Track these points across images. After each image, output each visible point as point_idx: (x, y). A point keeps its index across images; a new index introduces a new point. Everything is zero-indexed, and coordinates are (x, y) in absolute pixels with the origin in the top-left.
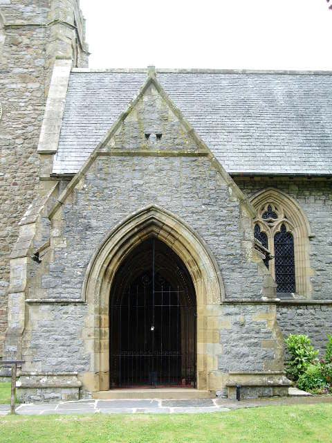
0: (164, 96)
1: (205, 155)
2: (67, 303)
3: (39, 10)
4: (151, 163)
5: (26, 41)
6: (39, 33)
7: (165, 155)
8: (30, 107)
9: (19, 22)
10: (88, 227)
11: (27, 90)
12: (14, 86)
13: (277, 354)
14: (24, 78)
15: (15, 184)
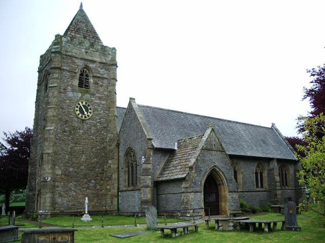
0: (215, 135)
1: (224, 151)
2: (198, 192)
3: (106, 72)
4: (214, 153)
5: (101, 83)
6: (105, 81)
7: (216, 151)
8: (102, 111)
9: (98, 75)
10: (201, 170)
11: (101, 103)
12: (96, 101)
13: (239, 205)
14: (100, 98)
15: (97, 142)
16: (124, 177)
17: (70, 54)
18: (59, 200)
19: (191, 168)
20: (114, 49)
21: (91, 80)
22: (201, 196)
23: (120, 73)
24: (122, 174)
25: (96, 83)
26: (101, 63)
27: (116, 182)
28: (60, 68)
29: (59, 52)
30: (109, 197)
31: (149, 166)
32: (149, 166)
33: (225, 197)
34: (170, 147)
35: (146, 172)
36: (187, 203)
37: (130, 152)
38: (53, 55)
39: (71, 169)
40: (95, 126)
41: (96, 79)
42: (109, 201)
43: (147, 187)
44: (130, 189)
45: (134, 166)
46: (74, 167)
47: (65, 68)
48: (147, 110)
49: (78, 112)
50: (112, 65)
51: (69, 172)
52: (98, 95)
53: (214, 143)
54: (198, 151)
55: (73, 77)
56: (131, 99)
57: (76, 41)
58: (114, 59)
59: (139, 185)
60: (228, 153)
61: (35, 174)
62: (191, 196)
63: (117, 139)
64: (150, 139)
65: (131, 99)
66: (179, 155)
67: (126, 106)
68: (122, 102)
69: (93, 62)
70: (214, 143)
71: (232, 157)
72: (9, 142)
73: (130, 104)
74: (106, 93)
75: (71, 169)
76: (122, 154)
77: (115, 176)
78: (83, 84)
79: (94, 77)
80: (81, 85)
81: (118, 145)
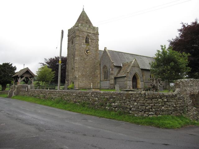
4: (136, 68)
6: (95, 41)
14: (93, 47)
16: (102, 76)
17: (82, 30)
18: (80, 84)
19: (128, 73)
20: (98, 28)
21: (90, 40)
22: (131, 82)
23: (100, 37)
24: (101, 75)
25: (91, 41)
26: (93, 33)
27: (99, 78)
28: (79, 36)
29: (78, 30)
30: (96, 83)
31: (113, 72)
32: (113, 72)
33: (139, 83)
34: (120, 65)
35: (112, 74)
36: (127, 84)
37: (105, 67)
38: (76, 31)
39: (84, 73)
40: (92, 57)
41: (91, 40)
42: (97, 85)
43: (112, 79)
44: (105, 80)
45: (107, 72)
46: (85, 73)
47: (80, 36)
48: (112, 52)
49: (86, 52)
50: (97, 34)
51: (83, 74)
52: (92, 46)
53: (136, 64)
54: (130, 68)
55: (83, 39)
56: (105, 48)
57: (84, 25)
58: (97, 32)
59: (109, 79)
60: (141, 68)
61: (68, 75)
62: (128, 82)
63: (99, 62)
64: (113, 63)
65: (105, 48)
66: (123, 68)
67: (103, 50)
68: (101, 48)
69: (90, 33)
70: (136, 64)
71: (142, 69)
72: (47, 63)
73: (105, 49)
74: (95, 45)
75: (84, 73)
76: (101, 68)
77: (99, 76)
78: (87, 42)
79: (91, 39)
80: (86, 42)
81: (100, 65)
